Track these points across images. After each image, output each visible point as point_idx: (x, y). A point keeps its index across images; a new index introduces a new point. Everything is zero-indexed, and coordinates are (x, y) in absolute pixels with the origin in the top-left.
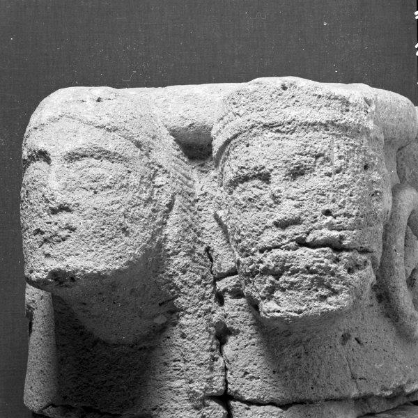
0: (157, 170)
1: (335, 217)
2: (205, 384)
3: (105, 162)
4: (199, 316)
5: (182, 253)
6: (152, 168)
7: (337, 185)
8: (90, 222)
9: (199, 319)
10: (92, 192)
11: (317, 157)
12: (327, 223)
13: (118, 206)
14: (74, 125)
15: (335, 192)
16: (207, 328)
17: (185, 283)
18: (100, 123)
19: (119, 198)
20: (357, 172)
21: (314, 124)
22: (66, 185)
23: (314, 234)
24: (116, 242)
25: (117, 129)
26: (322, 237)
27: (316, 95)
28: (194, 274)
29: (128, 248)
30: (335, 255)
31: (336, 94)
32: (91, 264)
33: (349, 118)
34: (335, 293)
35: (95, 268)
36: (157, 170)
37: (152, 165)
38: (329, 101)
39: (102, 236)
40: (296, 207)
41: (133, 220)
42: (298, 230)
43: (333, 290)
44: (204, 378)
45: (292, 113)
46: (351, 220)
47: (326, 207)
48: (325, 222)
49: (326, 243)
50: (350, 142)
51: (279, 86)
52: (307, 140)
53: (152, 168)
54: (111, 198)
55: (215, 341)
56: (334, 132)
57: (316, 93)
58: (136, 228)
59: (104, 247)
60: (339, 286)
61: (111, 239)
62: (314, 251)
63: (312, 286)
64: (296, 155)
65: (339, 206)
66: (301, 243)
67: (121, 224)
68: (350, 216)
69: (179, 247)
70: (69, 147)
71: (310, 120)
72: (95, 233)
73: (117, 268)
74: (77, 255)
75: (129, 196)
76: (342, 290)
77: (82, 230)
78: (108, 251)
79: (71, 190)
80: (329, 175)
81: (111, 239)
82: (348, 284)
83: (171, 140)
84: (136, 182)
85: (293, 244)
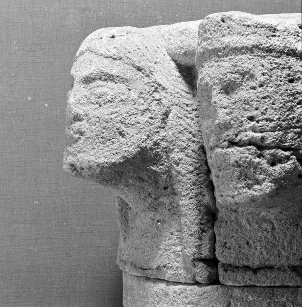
0: (157, 88)
1: (258, 122)
2: (194, 249)
3: (110, 83)
4: (191, 198)
5: (176, 150)
6: (153, 86)
7: (261, 96)
8: (94, 127)
9: (191, 200)
10: (97, 105)
11: (243, 75)
12: (250, 127)
13: (116, 115)
14: (92, 56)
15: (259, 102)
16: (197, 207)
17: (179, 173)
18: (109, 54)
19: (117, 109)
20: (280, 85)
21: (242, 48)
22: (80, 101)
23: (241, 136)
24: (113, 142)
25: (121, 58)
26: (247, 138)
27: (245, 25)
28: (187, 166)
29: (124, 146)
30: (259, 152)
31: (263, 24)
32: (93, 158)
33: (276, 42)
34: (258, 182)
35: (96, 161)
36: (157, 88)
37: (152, 84)
38: (256, 30)
39: (102, 138)
40: (228, 114)
41: (129, 125)
42: (231, 133)
43: (257, 180)
44: (193, 245)
45: (227, 40)
46: (272, 124)
47: (250, 114)
48: (249, 125)
49: (250, 143)
50: (275, 61)
51: (219, 19)
52: (236, 61)
53: (153, 86)
54: (111, 110)
55: (205, 217)
56: (259, 54)
57: (245, 23)
58: (131, 131)
59: (103, 146)
60: (262, 176)
61: (109, 140)
62: (241, 149)
63: (241, 176)
64: (228, 74)
65: (262, 113)
66: (232, 143)
67: (118, 129)
68: (271, 121)
69: (174, 145)
70: (85, 73)
71: (239, 45)
72: (97, 135)
73: (113, 161)
74: (84, 152)
75: (127, 108)
76: (264, 180)
77: (88, 134)
78: (107, 149)
79: (84, 104)
80: (254, 88)
81: (109, 140)
82: (270, 175)
83: (173, 65)
84: (135, 97)
85: (226, 143)
